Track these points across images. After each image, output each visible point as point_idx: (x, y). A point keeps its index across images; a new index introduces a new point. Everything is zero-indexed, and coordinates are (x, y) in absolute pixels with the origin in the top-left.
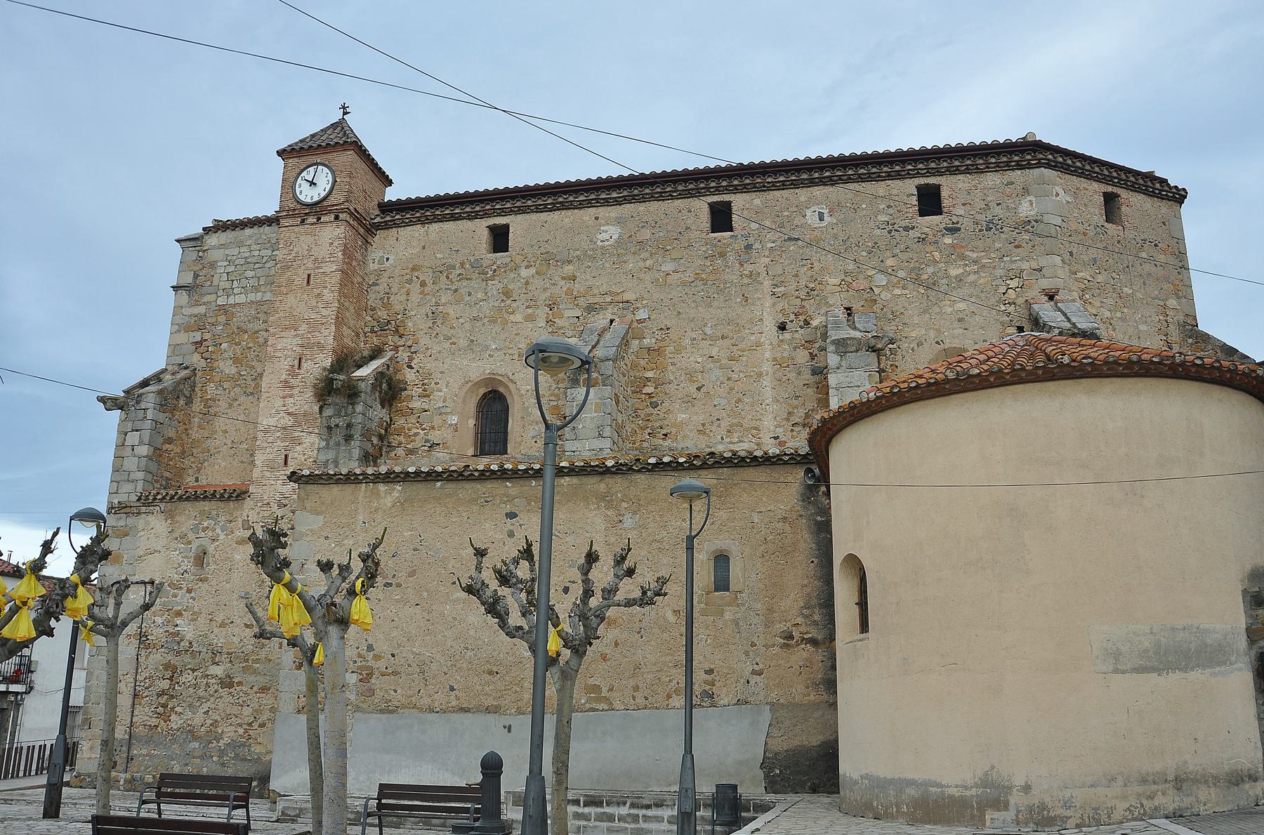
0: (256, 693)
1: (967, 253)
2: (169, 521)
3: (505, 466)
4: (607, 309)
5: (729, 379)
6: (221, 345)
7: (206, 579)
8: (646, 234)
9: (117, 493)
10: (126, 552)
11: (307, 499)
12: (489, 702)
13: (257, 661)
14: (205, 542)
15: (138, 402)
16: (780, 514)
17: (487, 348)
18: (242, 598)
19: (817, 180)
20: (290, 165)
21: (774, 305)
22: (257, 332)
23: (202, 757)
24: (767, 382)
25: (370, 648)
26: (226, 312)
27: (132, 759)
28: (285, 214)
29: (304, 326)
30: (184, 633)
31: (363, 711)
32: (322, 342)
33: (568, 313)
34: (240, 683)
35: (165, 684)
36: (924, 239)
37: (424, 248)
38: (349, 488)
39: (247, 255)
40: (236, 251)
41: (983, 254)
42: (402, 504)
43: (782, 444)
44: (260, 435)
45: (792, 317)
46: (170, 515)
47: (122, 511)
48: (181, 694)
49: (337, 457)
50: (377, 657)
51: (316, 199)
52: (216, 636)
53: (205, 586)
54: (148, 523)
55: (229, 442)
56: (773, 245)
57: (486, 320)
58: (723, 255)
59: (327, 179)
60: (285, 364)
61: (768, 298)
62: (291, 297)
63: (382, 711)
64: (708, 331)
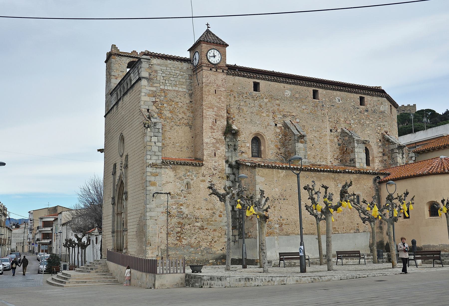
0: (212, 231)
1: (370, 118)
2: (174, 172)
3: (315, 168)
4: (289, 117)
5: (320, 144)
6: (164, 104)
7: (191, 193)
8: (297, 95)
9: (151, 159)
10: (158, 182)
11: (259, 172)
12: (312, 232)
13: (212, 221)
14: (189, 180)
15: (155, 125)
16: (369, 186)
17: (256, 123)
18: (205, 200)
19: (339, 90)
20: (204, 46)
21: (329, 124)
22: (178, 102)
23: (195, 253)
24: (328, 146)
25: (281, 217)
26: (164, 92)
27: (169, 256)
28: (205, 65)
29: (216, 108)
30: (184, 211)
31: (281, 235)
32: (223, 115)
33: (278, 116)
34: (206, 228)
35: (179, 229)
36: (361, 112)
37: (234, 84)
38: (271, 170)
39: (170, 71)
40: (165, 68)
41: (373, 119)
42: (286, 176)
43: (332, 163)
44: (205, 144)
45: (333, 128)
46: (174, 170)
47: (154, 166)
48: (186, 233)
49: (232, 155)
50: (283, 220)
51: (216, 63)
52: (196, 213)
53: (190, 195)
54: (165, 172)
55: (172, 142)
56: (328, 106)
57: (255, 114)
58: (317, 107)
59: (219, 56)
60: (211, 121)
61: (328, 121)
62: (210, 97)
63: (286, 235)
64: (314, 128)
